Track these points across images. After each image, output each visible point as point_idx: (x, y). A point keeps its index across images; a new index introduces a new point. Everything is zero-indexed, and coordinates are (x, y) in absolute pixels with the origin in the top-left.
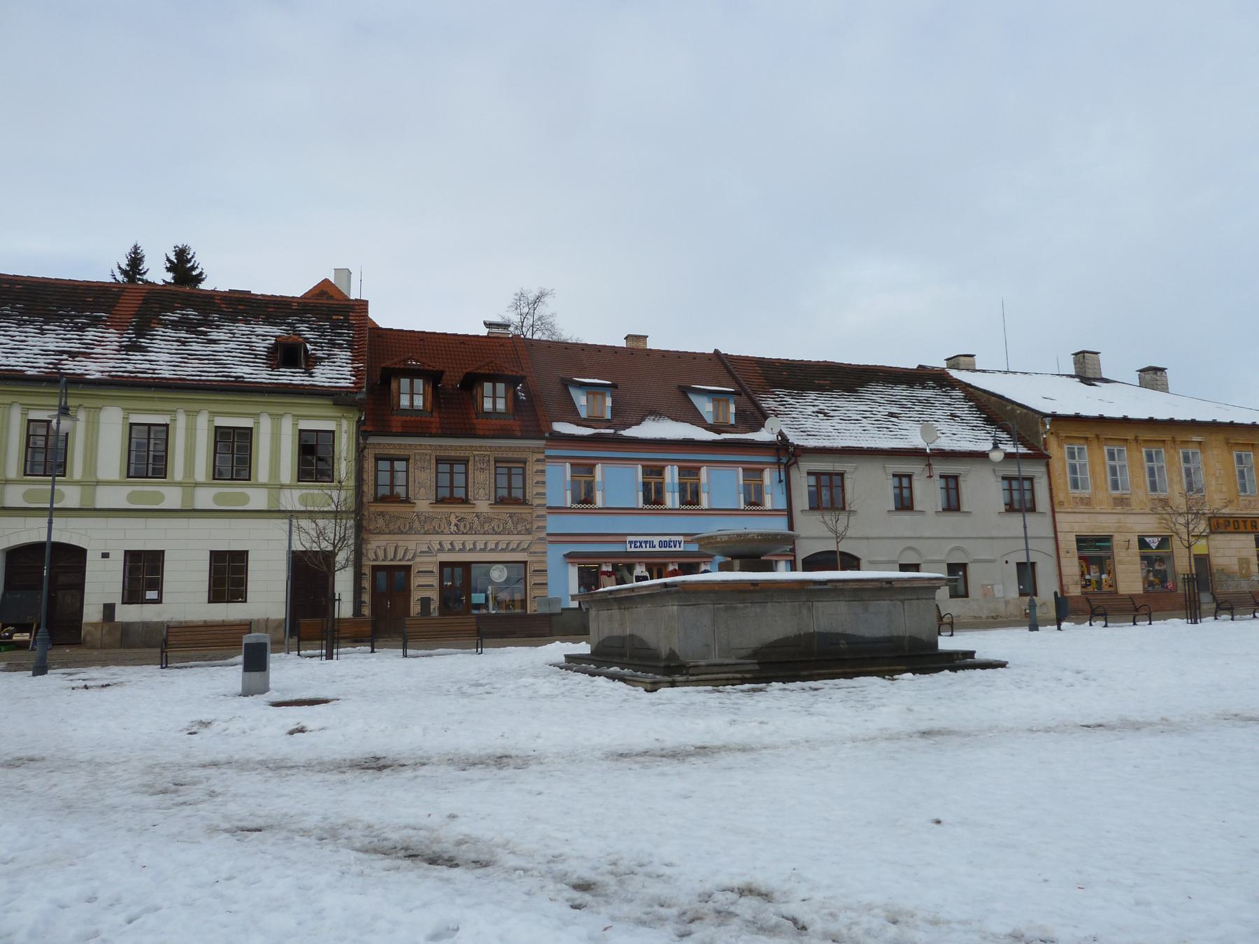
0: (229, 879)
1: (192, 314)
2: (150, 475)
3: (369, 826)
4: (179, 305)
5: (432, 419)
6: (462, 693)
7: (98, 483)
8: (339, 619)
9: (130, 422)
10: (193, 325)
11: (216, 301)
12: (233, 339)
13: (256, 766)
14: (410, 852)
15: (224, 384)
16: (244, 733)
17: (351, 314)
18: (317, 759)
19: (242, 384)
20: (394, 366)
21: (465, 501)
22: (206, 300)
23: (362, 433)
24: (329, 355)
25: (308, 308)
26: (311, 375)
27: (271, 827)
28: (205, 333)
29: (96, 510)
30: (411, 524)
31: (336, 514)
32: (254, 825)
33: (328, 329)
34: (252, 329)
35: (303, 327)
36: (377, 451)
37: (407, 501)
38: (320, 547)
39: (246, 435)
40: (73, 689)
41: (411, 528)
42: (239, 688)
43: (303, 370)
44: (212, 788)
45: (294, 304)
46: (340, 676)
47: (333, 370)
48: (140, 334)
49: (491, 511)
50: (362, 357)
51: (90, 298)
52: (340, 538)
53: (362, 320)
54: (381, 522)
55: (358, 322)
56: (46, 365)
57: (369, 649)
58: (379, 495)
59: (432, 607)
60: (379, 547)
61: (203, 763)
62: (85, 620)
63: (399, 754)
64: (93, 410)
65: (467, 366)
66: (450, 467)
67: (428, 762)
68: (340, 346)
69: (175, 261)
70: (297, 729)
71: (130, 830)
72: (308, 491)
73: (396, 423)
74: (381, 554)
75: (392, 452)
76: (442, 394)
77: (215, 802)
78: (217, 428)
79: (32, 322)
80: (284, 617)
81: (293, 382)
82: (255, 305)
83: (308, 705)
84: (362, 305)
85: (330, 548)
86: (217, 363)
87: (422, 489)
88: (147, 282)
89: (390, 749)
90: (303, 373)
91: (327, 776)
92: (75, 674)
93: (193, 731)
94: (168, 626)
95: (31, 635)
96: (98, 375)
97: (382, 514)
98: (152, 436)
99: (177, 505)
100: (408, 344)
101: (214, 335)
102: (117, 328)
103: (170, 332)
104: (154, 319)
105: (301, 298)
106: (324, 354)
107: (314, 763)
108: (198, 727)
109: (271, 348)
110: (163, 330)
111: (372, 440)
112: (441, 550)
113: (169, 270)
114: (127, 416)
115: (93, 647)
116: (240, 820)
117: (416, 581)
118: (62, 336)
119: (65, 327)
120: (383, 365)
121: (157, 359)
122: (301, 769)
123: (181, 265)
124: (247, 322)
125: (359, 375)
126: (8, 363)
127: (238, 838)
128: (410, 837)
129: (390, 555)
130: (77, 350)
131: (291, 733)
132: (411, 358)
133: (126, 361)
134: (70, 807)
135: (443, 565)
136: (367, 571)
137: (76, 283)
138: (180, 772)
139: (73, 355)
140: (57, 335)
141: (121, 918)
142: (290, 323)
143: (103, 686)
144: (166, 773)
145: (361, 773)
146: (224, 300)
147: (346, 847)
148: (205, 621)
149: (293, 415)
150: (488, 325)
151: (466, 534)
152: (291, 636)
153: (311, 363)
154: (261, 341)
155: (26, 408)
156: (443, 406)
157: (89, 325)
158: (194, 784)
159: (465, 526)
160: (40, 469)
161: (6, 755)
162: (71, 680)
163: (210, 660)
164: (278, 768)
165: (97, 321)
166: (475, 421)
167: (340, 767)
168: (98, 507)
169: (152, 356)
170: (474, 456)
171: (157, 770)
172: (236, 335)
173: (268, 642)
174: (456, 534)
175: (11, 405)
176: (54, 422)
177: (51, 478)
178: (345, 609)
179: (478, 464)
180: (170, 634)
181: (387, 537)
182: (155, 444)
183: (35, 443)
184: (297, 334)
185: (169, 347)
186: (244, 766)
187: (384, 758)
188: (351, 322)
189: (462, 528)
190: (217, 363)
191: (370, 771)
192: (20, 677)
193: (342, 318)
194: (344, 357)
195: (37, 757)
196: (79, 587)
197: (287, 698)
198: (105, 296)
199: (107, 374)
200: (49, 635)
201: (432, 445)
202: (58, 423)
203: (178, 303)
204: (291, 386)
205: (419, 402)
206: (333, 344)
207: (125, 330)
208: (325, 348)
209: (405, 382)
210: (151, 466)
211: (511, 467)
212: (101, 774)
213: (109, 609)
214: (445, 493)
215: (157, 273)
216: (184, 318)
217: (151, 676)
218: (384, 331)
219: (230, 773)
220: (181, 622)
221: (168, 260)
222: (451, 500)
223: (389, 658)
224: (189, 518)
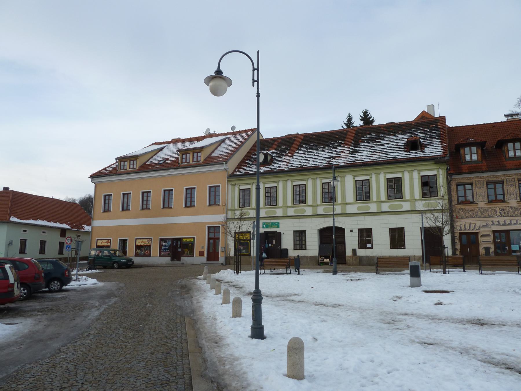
0: (424, 363)
1: (373, 135)
2: (364, 199)
3: (483, 351)
4: (368, 133)
5: (483, 164)
6: (516, 293)
7: (347, 204)
8: (448, 256)
9: (294, 184)
10: (374, 140)
11: (382, 129)
12: (390, 142)
13: (424, 317)
14: (507, 366)
15: (388, 161)
16: (416, 302)
17: (438, 123)
18: (450, 317)
19: (396, 160)
20: (461, 143)
21: (504, 201)
22: (378, 129)
23: (449, 174)
24: (430, 142)
25: (419, 124)
26: (423, 152)
27: (437, 344)
28: (379, 142)
29: (317, 215)
30: (477, 213)
31: (442, 210)
32: (429, 342)
33: (429, 132)
34: (397, 137)
35: (418, 133)
36: (457, 182)
37: (473, 203)
38: (436, 224)
39: (399, 180)
40: (347, 280)
41: (477, 215)
42: (409, 284)
43: (420, 151)
44: (408, 324)
45: (413, 124)
46: (452, 281)
47: (433, 149)
48: (356, 147)
49: (486, 206)
50: (445, 141)
51: (337, 136)
52: (445, 221)
53: (444, 125)
54: (461, 213)
55: (442, 126)
56: (326, 163)
57: (462, 270)
58: (460, 201)
59: (491, 251)
60: (462, 224)
61: (402, 313)
62: (346, 255)
63: (490, 319)
64: (342, 177)
65: (498, 137)
66: (464, 187)
67: (506, 324)
68: (435, 138)
69: (363, 116)
70: (438, 303)
71: (380, 336)
72: (429, 201)
73: (465, 168)
74: (463, 228)
75: (464, 181)
76: (486, 152)
77: (410, 330)
78: (387, 179)
79: (320, 148)
80: (421, 255)
81: (416, 156)
82: (397, 127)
83: (441, 293)
84: (443, 118)
85: (441, 225)
86: (385, 153)
87: (481, 197)
88: (354, 127)
89: (485, 316)
90: (420, 152)
91: (457, 325)
92: (347, 275)
93: (395, 300)
94: (377, 258)
95: (329, 260)
96: (343, 164)
97: (462, 210)
98: (364, 184)
99: (311, 214)
100: (468, 130)
101: (383, 142)
102: (348, 145)
103: (366, 144)
104: (360, 140)
105: (414, 121)
106: (428, 142)
107: (449, 318)
108: (396, 298)
109: (406, 143)
110: (363, 143)
111: (454, 177)
112: (493, 224)
113: (361, 120)
114: (419, 173)
115: (350, 265)
116: (423, 339)
117: (481, 239)
118: (330, 151)
119: (330, 148)
120: (455, 143)
121: (363, 155)
122: (444, 320)
123: (366, 118)
124: (395, 135)
125: (445, 149)
126: (314, 164)
127: (424, 346)
128: (506, 359)
129: (468, 228)
130: (335, 156)
131: (436, 304)
132: (469, 138)
133: (352, 157)
134: (356, 324)
135: (494, 232)
136: (457, 235)
137: (332, 132)
138: (393, 316)
139: (334, 158)
140: (328, 151)
141: (385, 371)
142: (412, 132)
143: (357, 280)
144: (388, 316)
145: (473, 326)
146: (384, 128)
147: (474, 358)
148: (390, 256)
149: (418, 170)
150: (506, 116)
151: (506, 216)
152: (426, 262)
153: (423, 147)
154: (401, 141)
155: (293, 181)
156: (487, 157)
157: (338, 146)
158: (400, 321)
159: (505, 213)
160: (327, 200)
161: (331, 302)
162: (346, 277)
163: (394, 272)
164: (434, 319)
165: (340, 144)
166: (505, 163)
167: (462, 322)
168: (318, 214)
169: (361, 154)
170: (506, 180)
171: (384, 314)
172: (391, 141)
173: (420, 265)
174: (500, 217)
175: (316, 178)
176: (332, 182)
177: (332, 203)
178: (449, 252)
179: (478, 185)
180: (378, 261)
181: (465, 220)
182: (365, 187)
183: (325, 191)
184: (415, 136)
185: (366, 149)
186: (419, 316)
187: (483, 320)
188: (439, 127)
189: (503, 214)
190: (385, 153)
191: (477, 325)
192: (329, 275)
193: (434, 126)
194: (437, 142)
195: (341, 304)
196: (343, 243)
197: (430, 289)
198: (342, 134)
199: (346, 163)
200: (337, 260)
201: (484, 176)
202: (333, 183)
203: (368, 132)
204: (416, 158)
205: (475, 157)
206: (432, 138)
207: (350, 146)
208: (428, 140)
209: (467, 149)
210: (364, 196)
211: (496, 184)
212: (364, 313)
213: (354, 251)
214: (493, 198)
215: (357, 123)
216: (371, 137)
217: (373, 277)
218: (476, 126)
219: (414, 319)
220: (381, 256)
221: (361, 116)
222: (496, 201)
223: (473, 274)
224: (380, 215)
